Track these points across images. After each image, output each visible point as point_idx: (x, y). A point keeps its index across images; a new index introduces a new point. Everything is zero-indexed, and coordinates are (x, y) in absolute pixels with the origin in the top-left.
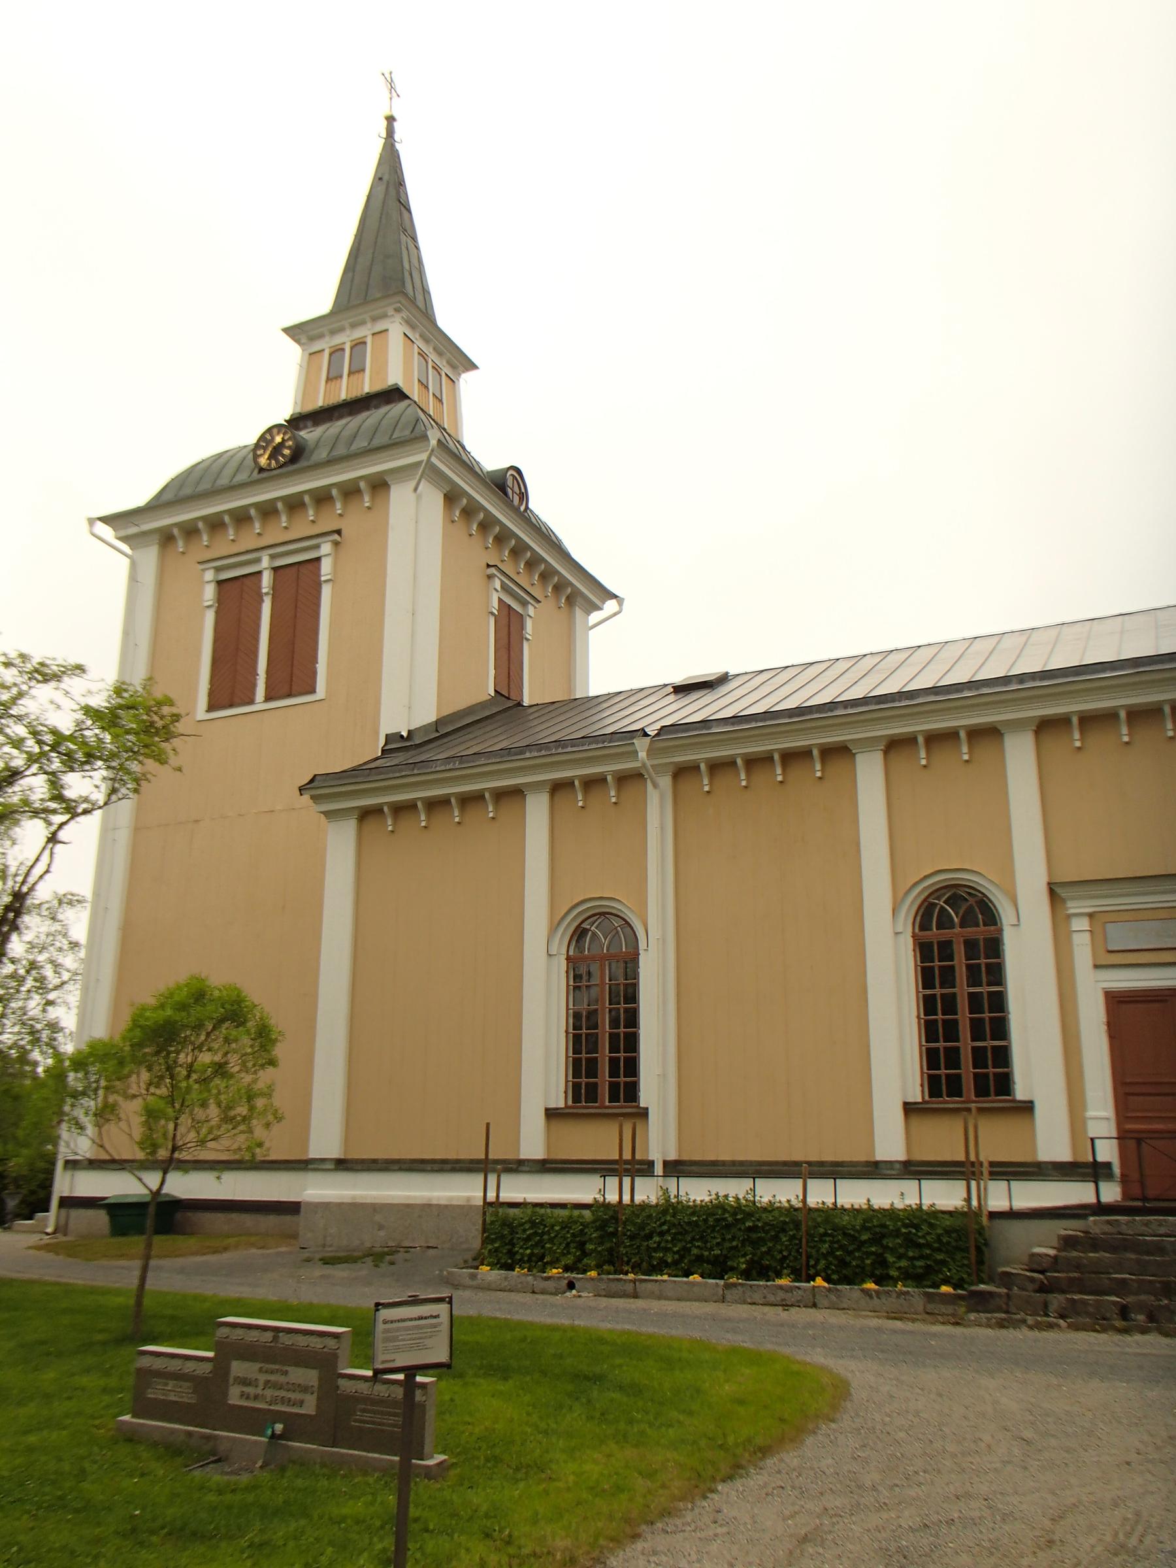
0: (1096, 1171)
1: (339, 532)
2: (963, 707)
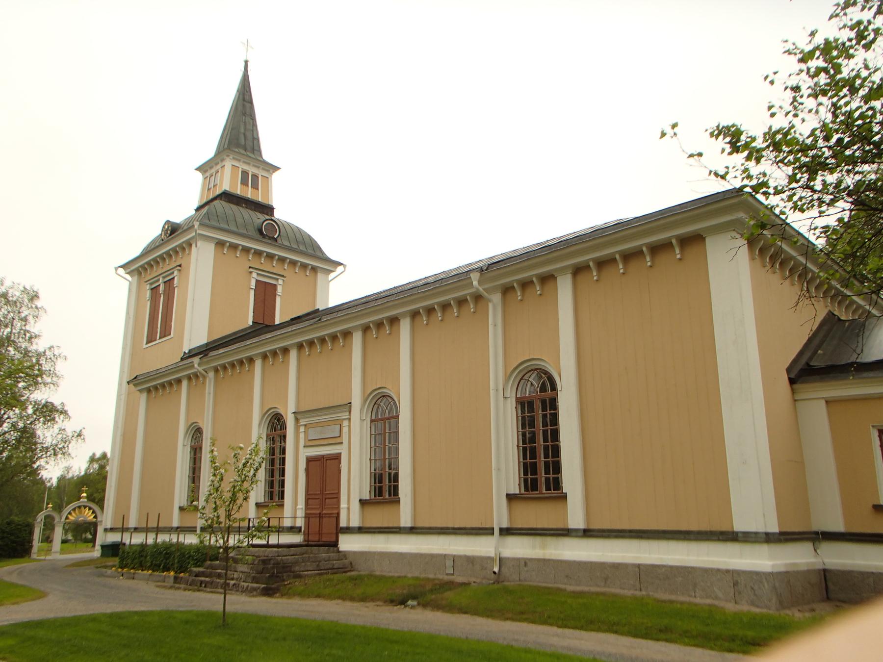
0: (298, 530)
1: (180, 266)
2: (343, 320)
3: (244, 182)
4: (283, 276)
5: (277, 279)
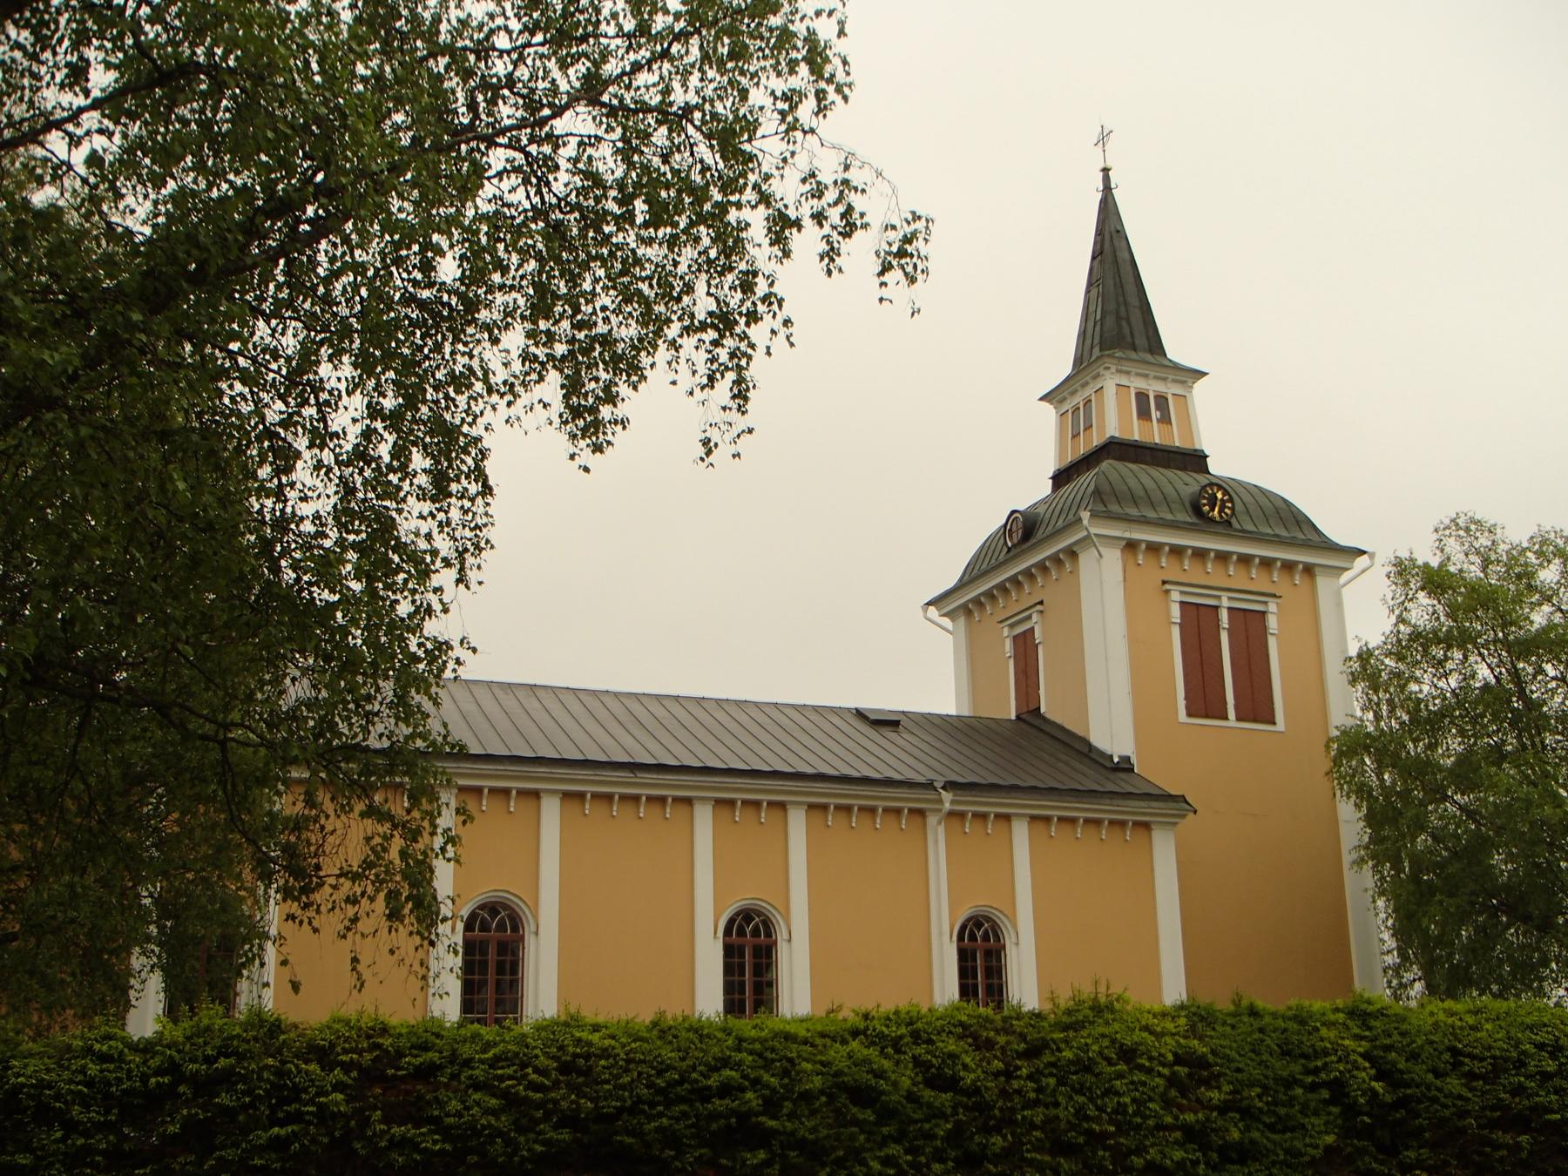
1: (1041, 603)
3: (1144, 413)
4: (1274, 596)
5: (1266, 603)
